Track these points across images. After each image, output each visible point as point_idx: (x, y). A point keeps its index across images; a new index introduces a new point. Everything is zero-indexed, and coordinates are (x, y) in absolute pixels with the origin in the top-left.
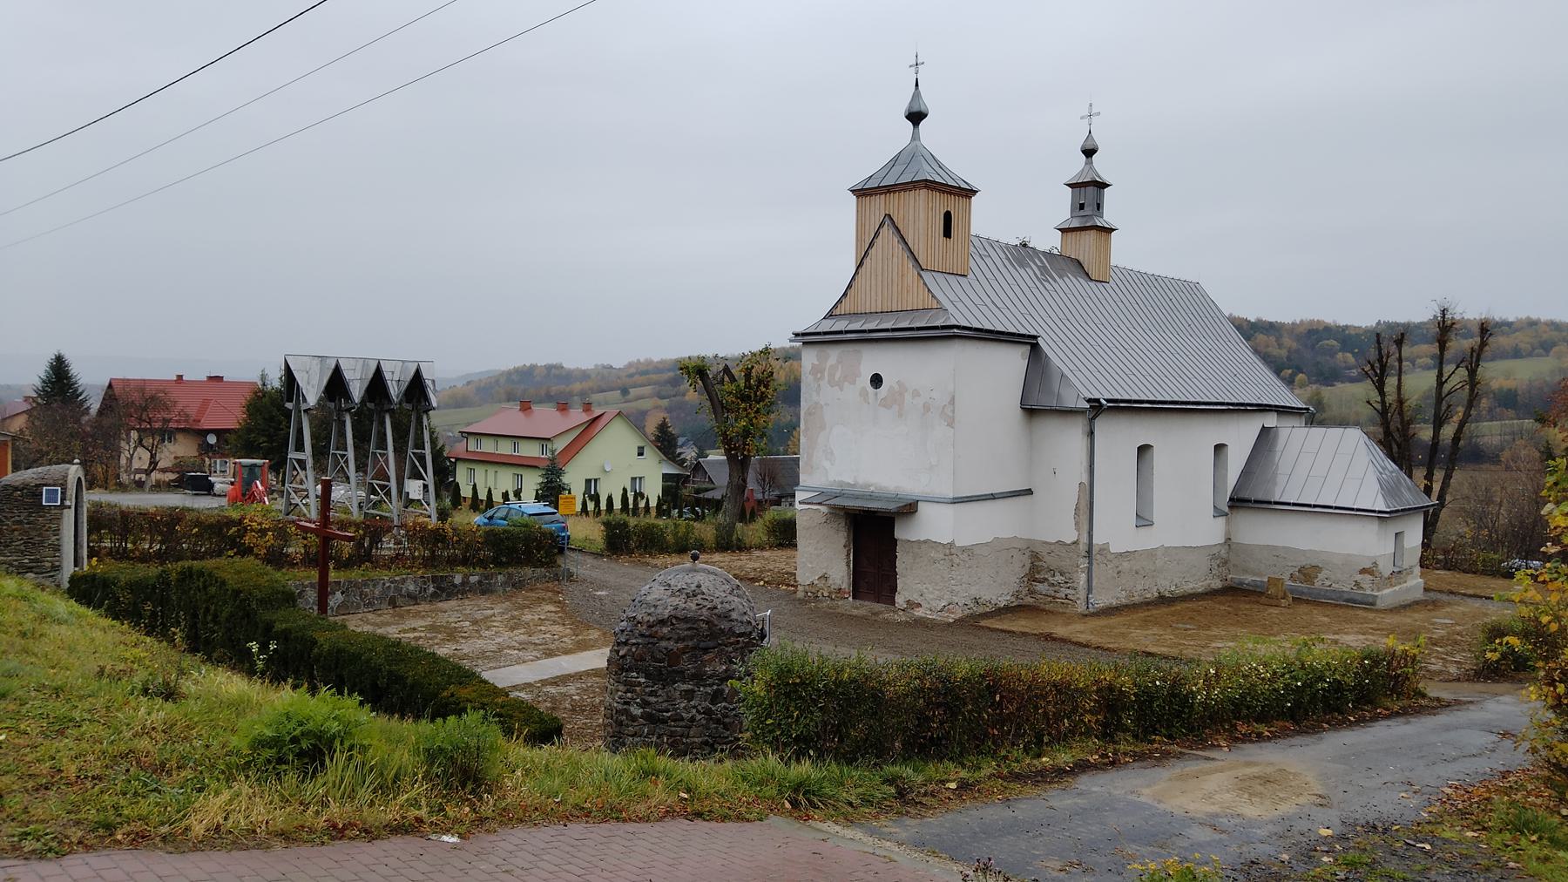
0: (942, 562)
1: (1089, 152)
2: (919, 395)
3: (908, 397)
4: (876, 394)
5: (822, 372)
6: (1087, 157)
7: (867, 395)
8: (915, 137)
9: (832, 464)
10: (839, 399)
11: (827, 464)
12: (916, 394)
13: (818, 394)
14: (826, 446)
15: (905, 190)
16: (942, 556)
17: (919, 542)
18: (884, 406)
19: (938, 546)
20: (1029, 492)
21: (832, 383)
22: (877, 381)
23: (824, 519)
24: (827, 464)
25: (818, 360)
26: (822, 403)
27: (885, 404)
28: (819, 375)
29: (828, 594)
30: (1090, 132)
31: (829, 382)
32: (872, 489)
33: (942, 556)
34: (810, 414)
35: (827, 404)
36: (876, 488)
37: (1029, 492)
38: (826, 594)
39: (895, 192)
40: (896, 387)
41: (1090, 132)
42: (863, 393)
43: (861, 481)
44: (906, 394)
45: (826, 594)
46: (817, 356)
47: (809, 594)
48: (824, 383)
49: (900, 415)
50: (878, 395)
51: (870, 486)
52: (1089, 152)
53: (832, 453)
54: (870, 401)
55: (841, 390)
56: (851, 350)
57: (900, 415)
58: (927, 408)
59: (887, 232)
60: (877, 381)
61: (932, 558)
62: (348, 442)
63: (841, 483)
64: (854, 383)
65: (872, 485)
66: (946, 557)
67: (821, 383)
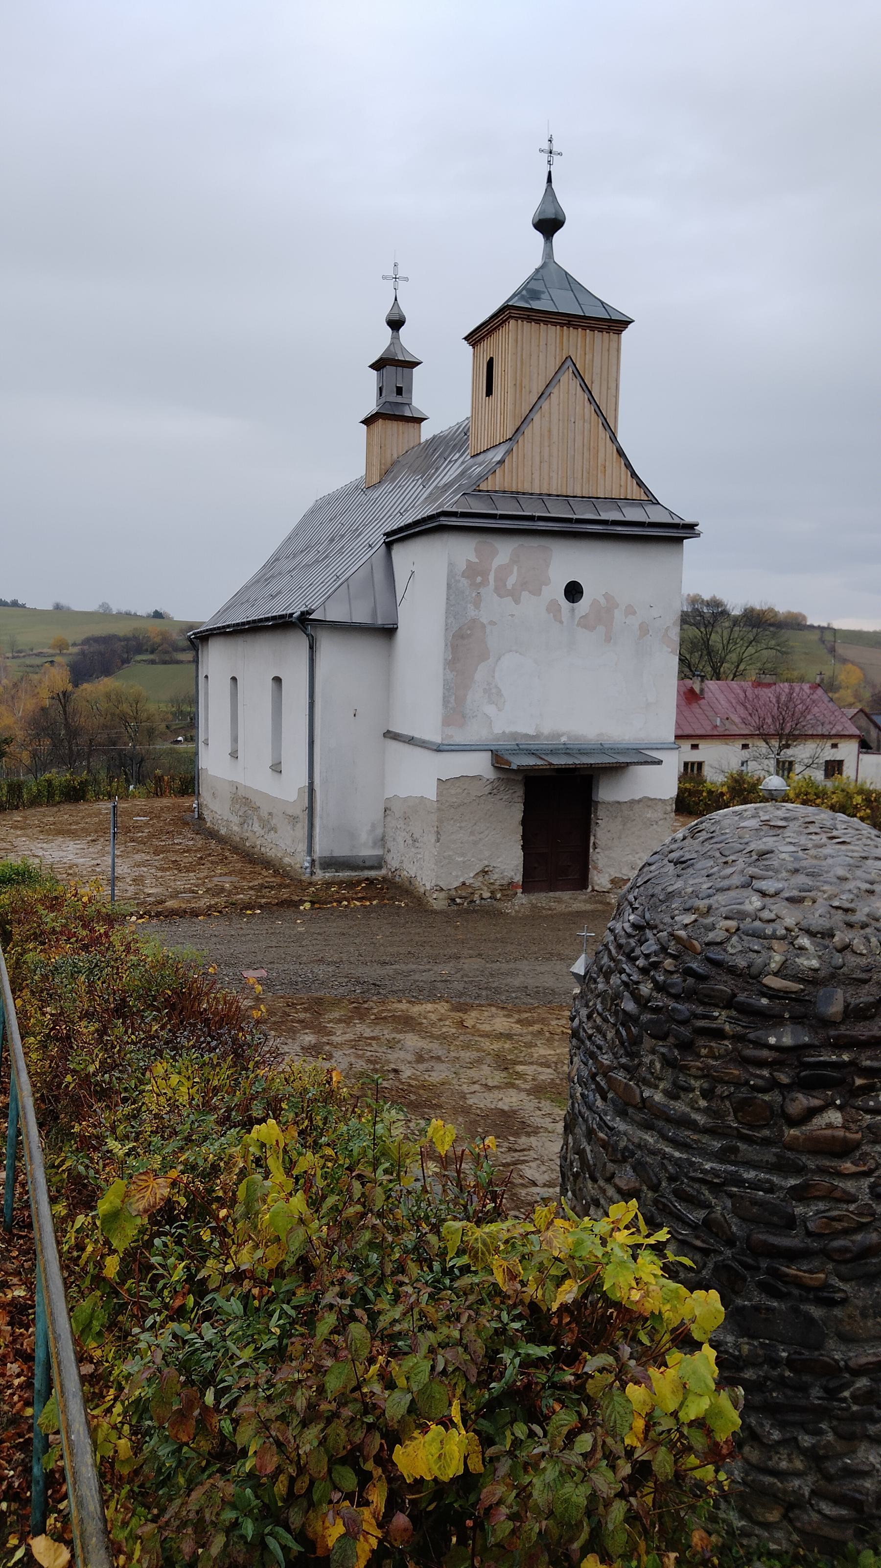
0: (660, 823)
1: (396, 324)
2: (634, 613)
3: (618, 614)
4: (573, 610)
5: (485, 574)
6: (393, 329)
7: (560, 611)
8: (549, 253)
9: (500, 710)
10: (512, 615)
11: (490, 710)
12: (630, 611)
13: (477, 606)
14: (489, 684)
15: (593, 329)
16: (661, 816)
17: (633, 802)
18: (585, 627)
19: (656, 804)
20: (391, 735)
21: (501, 590)
22: (573, 591)
23: (489, 788)
24: (490, 710)
25: (477, 557)
26: (484, 620)
27: (585, 623)
28: (479, 579)
29: (489, 895)
30: (396, 299)
31: (496, 590)
32: (564, 739)
33: (661, 816)
34: (462, 637)
35: (492, 623)
36: (569, 738)
37: (391, 735)
38: (487, 895)
39: (576, 327)
40: (603, 601)
41: (396, 299)
42: (553, 608)
43: (546, 730)
44: (616, 611)
45: (487, 895)
46: (476, 550)
47: (458, 900)
48: (488, 592)
49: (608, 639)
50: (576, 611)
51: (562, 735)
52: (396, 324)
53: (499, 693)
54: (563, 619)
55: (517, 601)
56: (536, 545)
57: (608, 639)
58: (644, 629)
59: (567, 377)
60: (573, 591)
61: (649, 819)
62: (53, 1288)
63: (514, 735)
64: (537, 592)
65: (562, 735)
66: (667, 816)
67: (482, 590)
